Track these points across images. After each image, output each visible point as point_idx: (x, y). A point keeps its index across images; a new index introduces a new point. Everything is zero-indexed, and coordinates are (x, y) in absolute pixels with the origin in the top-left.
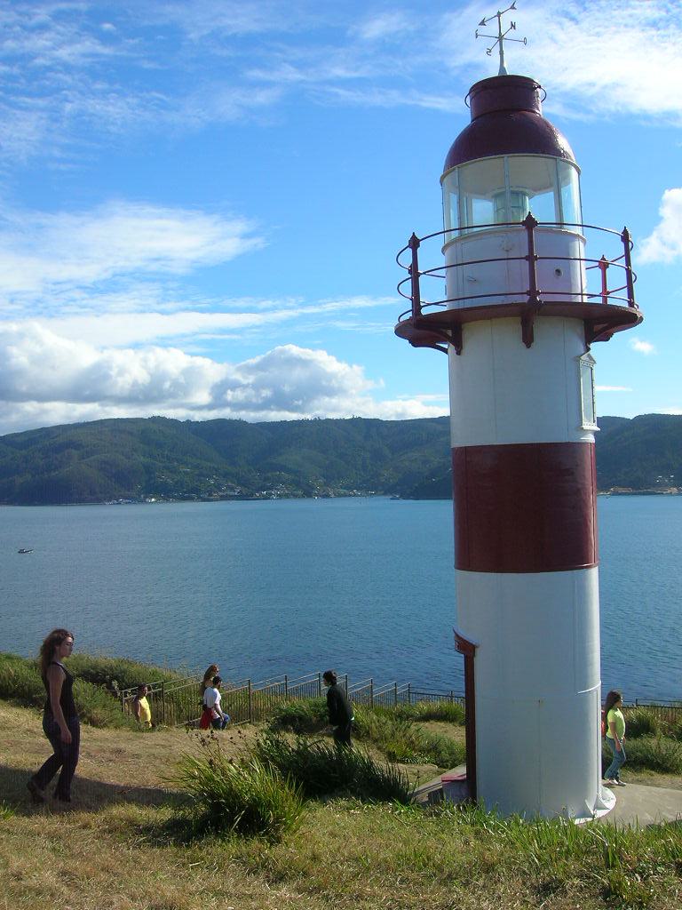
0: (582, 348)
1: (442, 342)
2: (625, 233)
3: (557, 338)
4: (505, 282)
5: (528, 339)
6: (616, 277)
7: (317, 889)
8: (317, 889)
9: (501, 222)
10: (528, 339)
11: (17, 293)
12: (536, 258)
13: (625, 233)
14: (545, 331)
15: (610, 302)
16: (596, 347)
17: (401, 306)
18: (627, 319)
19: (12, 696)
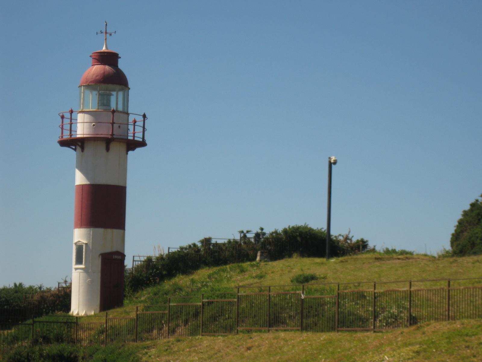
0: (125, 152)
1: (73, 146)
2: (97, 34)
3: (117, 148)
4: (105, 132)
5: (108, 149)
6: (139, 129)
7: (214, 318)
8: (214, 318)
9: (106, 134)
10: (108, 149)
11: (77, 242)
12: (115, 123)
13: (97, 34)
14: (114, 146)
15: (136, 139)
16: (130, 153)
17: (170, 247)
18: (143, 144)
19: (240, 319)
